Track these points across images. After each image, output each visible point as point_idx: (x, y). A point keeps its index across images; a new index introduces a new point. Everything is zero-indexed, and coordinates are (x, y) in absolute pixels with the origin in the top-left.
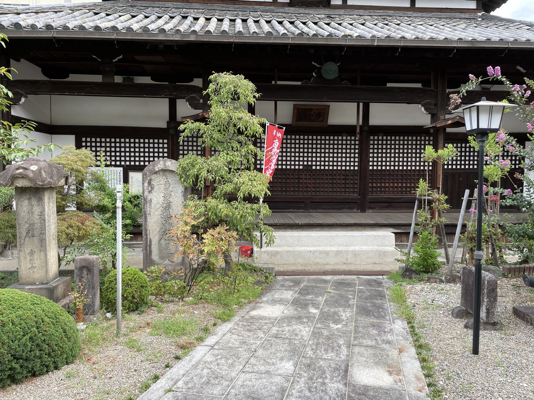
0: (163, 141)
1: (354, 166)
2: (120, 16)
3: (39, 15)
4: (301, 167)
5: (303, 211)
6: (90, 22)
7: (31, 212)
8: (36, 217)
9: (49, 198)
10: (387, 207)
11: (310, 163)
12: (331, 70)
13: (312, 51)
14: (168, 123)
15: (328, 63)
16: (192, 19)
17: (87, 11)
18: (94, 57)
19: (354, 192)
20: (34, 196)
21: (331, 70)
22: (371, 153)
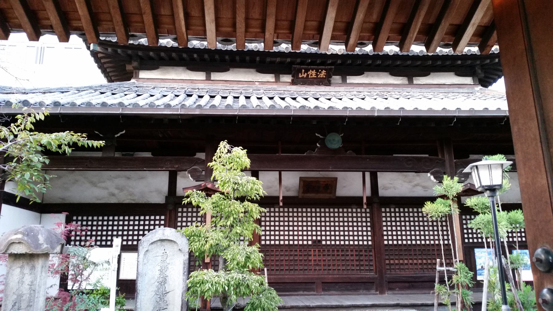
0: (160, 218)
1: (367, 240)
2: (126, 95)
3: (46, 94)
4: (310, 243)
5: (315, 293)
6: (96, 99)
7: (21, 282)
8: (25, 289)
9: (42, 267)
10: (409, 288)
11: (319, 238)
12: (335, 141)
13: (314, 122)
14: (167, 198)
15: (331, 134)
16: (197, 97)
17: (93, 91)
18: (96, 132)
19: (371, 270)
20: (28, 264)
21: (335, 141)
22: (385, 226)
